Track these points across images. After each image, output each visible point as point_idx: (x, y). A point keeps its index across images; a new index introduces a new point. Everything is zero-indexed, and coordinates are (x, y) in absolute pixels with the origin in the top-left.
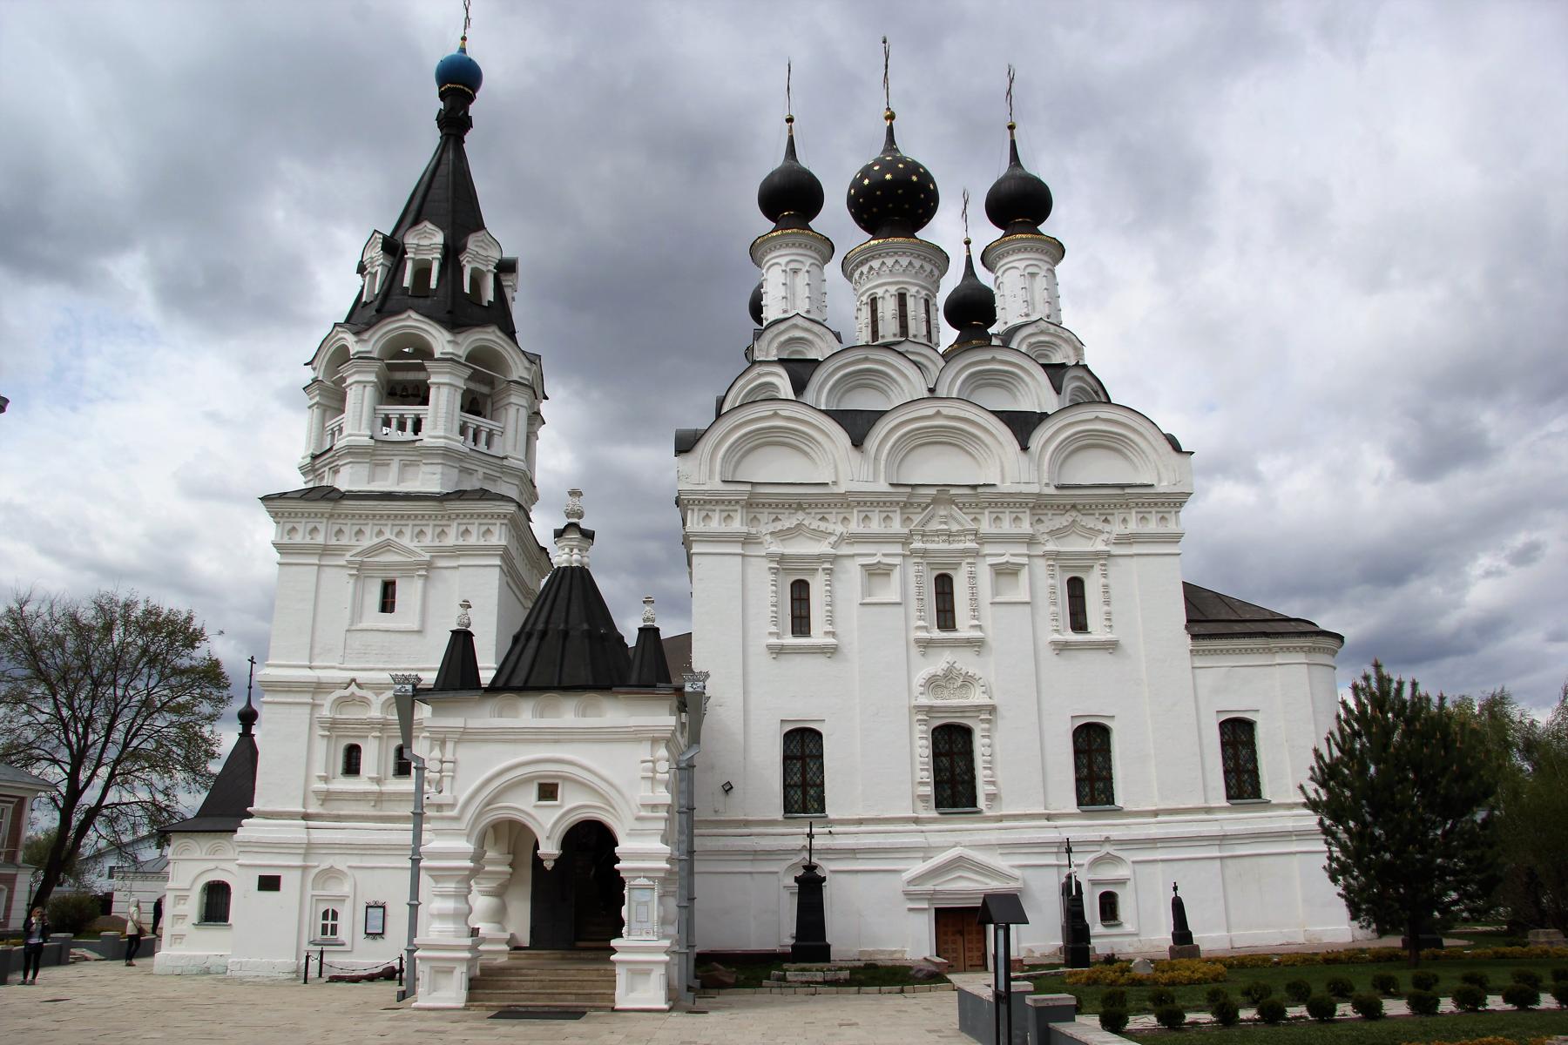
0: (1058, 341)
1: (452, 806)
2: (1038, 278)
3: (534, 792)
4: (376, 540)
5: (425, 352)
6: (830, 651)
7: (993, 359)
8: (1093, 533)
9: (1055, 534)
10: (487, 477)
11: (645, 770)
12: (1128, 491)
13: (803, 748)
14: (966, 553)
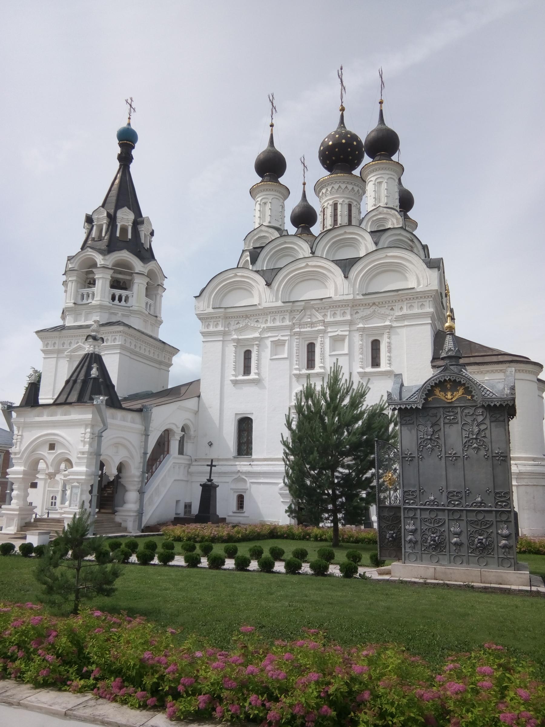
0: (388, 217)
1: (19, 453)
2: (383, 185)
3: (47, 447)
4: (76, 345)
5: (95, 265)
6: (257, 382)
7: (345, 233)
8: (384, 317)
9: (365, 319)
10: (123, 315)
11: (82, 437)
12: (400, 292)
13: (245, 425)
14: (319, 331)
